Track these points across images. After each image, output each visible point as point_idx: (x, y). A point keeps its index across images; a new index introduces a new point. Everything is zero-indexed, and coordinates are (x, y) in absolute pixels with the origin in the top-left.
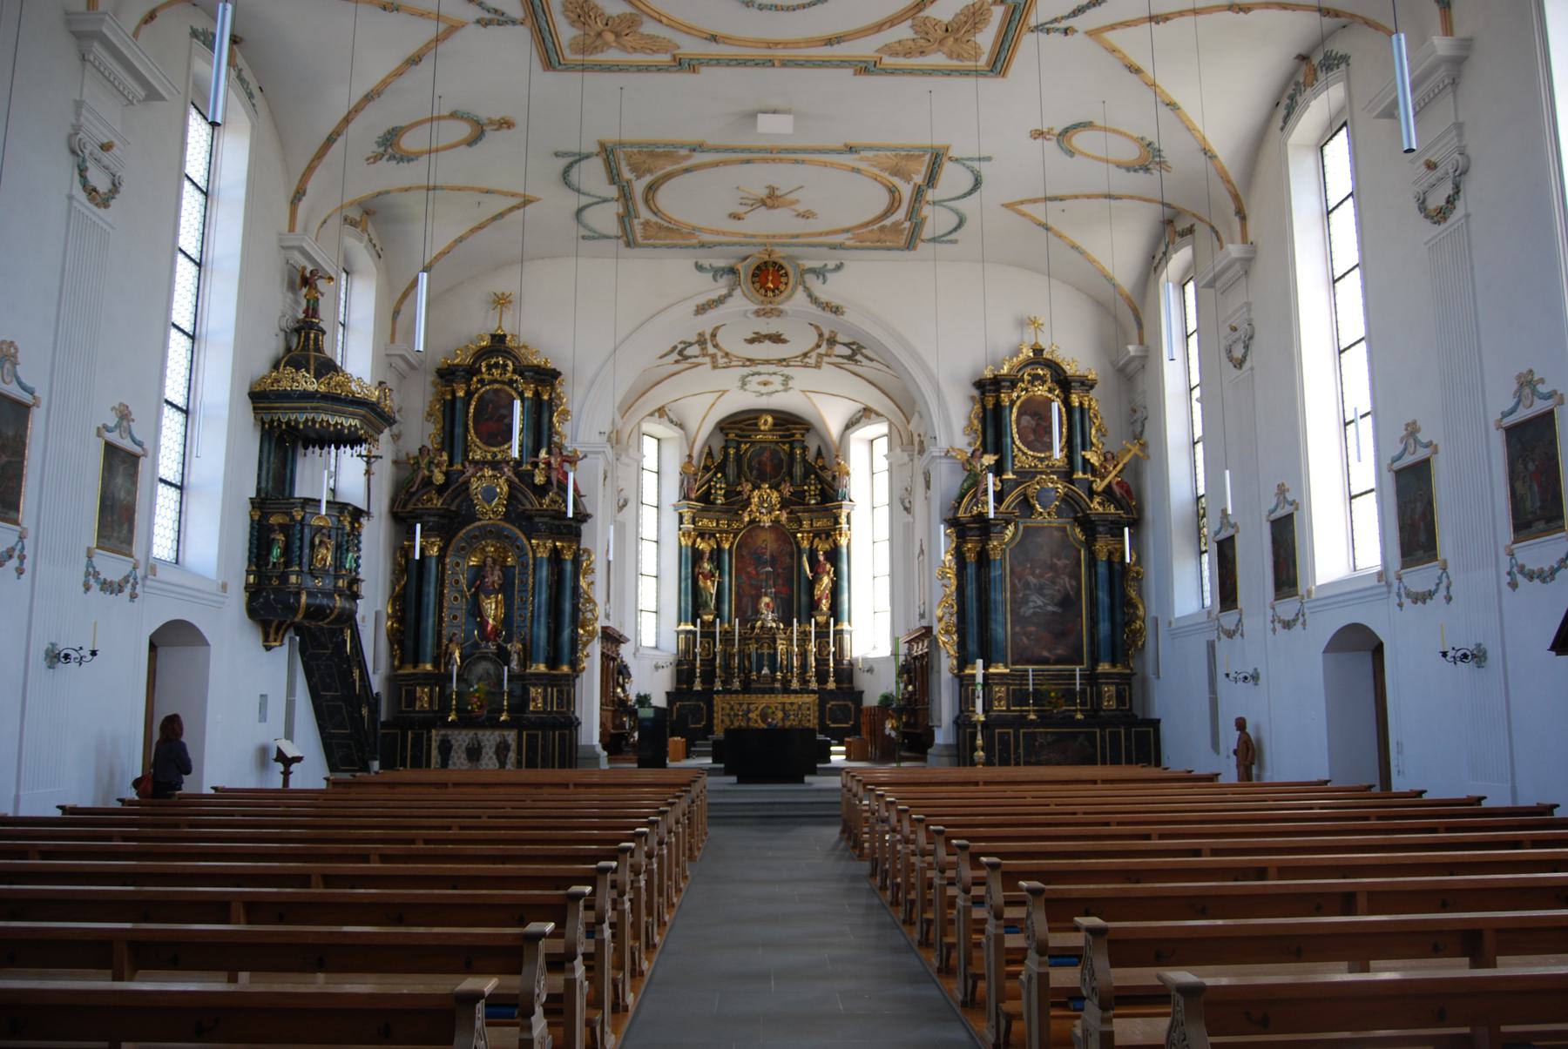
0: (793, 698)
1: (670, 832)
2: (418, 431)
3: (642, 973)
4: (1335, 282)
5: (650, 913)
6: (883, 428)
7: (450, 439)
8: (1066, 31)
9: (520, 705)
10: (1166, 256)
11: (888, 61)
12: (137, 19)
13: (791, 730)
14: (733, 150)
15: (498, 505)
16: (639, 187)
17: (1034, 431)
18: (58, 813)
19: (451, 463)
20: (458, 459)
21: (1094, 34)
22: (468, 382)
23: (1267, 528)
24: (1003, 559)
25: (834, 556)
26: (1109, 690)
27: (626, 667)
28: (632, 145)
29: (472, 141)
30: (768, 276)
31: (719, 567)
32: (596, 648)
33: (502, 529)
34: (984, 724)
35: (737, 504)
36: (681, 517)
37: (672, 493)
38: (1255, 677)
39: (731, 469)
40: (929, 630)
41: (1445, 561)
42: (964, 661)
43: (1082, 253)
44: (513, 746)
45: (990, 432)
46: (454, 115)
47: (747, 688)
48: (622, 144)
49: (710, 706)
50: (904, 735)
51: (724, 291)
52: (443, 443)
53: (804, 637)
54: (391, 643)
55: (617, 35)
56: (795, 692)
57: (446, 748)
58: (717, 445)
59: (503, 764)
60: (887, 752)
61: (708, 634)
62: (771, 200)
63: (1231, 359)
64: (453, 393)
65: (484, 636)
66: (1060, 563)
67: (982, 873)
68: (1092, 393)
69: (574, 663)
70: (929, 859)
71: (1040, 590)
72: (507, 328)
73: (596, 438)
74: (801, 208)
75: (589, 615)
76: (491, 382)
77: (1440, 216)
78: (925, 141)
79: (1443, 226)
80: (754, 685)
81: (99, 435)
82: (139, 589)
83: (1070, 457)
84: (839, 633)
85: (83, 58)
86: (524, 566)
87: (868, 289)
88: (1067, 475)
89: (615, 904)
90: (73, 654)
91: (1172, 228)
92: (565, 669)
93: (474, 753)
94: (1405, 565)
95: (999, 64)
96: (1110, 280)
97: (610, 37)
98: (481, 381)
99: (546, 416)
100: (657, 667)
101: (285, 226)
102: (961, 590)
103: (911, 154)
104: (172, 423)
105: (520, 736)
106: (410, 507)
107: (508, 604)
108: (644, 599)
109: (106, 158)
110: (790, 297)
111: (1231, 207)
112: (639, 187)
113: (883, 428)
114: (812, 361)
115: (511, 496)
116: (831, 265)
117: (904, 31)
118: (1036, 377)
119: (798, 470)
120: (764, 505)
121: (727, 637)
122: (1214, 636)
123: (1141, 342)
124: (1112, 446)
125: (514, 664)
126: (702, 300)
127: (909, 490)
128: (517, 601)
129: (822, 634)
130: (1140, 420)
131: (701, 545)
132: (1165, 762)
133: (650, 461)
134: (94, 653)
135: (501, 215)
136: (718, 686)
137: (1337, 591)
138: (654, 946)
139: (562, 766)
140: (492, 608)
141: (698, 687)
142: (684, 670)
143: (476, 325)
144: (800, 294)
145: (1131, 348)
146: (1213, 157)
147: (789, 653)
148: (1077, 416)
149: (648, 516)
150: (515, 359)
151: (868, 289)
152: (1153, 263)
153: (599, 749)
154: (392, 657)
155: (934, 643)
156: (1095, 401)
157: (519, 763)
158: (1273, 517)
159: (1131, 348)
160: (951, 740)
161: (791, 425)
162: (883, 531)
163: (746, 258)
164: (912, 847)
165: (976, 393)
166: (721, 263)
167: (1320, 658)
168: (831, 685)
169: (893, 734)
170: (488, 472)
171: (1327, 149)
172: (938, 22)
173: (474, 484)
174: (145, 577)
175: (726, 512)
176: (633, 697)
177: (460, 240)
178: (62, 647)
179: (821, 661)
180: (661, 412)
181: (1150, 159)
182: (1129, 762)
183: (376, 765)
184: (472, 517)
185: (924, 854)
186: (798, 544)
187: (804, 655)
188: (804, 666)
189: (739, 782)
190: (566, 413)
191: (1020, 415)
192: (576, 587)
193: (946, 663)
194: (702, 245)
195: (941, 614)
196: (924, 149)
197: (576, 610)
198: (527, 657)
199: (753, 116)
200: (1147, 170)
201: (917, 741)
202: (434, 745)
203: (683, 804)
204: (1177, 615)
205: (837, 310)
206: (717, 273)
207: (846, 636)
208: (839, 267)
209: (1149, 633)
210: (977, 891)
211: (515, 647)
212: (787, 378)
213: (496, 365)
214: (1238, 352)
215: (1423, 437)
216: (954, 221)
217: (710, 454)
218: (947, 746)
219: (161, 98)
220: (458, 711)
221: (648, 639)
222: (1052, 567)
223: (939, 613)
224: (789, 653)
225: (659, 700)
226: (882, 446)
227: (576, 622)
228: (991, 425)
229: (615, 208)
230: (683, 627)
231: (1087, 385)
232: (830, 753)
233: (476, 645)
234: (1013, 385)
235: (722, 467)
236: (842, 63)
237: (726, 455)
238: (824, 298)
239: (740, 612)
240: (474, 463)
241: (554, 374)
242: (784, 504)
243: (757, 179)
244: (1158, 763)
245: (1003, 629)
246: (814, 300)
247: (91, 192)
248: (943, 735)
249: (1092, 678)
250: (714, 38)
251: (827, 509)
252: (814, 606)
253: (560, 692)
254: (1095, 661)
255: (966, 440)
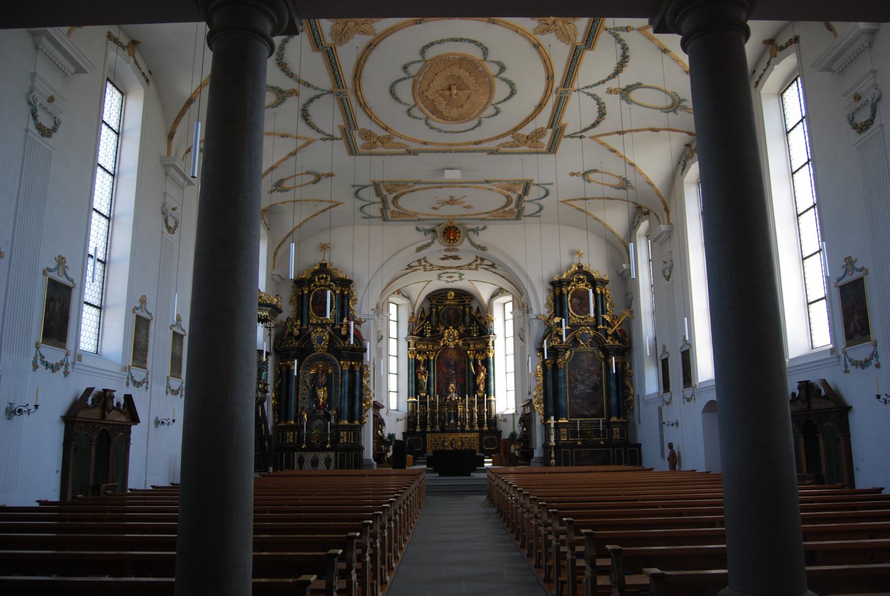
0: (466, 435)
1: (395, 514)
2: (288, 311)
3: (386, 583)
4: (793, 173)
5: (383, 563)
6: (510, 298)
7: (301, 313)
8: (581, 137)
9: (336, 440)
10: (638, 223)
11: (502, 149)
12: (185, 150)
13: (466, 450)
14: (434, 183)
15: (324, 345)
16: (390, 198)
17: (579, 305)
18: (37, 505)
19: (302, 325)
20: (305, 323)
21: (592, 138)
22: (309, 286)
23: (680, 355)
24: (565, 367)
25: (486, 362)
26: (616, 430)
27: (383, 420)
28: (388, 182)
29: (314, 183)
30: (451, 233)
31: (428, 369)
32: (371, 413)
33: (326, 356)
34: (555, 447)
35: (436, 336)
36: (409, 343)
37: (404, 332)
38: (677, 424)
39: (434, 319)
40: (531, 400)
41: (876, 341)
42: (546, 417)
43: (600, 221)
44: (333, 460)
45: (558, 307)
46: (307, 173)
47: (443, 430)
48: (383, 182)
49: (425, 439)
50: (522, 453)
51: (430, 241)
52: (297, 315)
53: (472, 403)
54: (274, 412)
55: (382, 143)
56: (467, 432)
57: (301, 461)
58: (427, 307)
59: (328, 468)
60: (512, 461)
61: (423, 402)
62: (452, 201)
63: (665, 276)
64: (302, 292)
65: (318, 407)
66: (592, 369)
67: (564, 528)
68: (607, 287)
69: (361, 420)
70: (549, 528)
71: (583, 382)
72: (327, 260)
73: (371, 312)
74: (465, 205)
75: (367, 397)
76: (320, 286)
77: (861, 128)
78: (520, 178)
79: (863, 135)
80: (447, 429)
81: (133, 312)
82: (70, 368)
83: (596, 316)
84: (489, 402)
85: (37, 47)
86: (337, 374)
87: (499, 238)
88: (595, 327)
89: (373, 545)
90: (24, 409)
91: (639, 212)
92: (357, 422)
93: (315, 463)
94: (685, 387)
95: (552, 148)
96: (613, 232)
97: (379, 144)
98: (315, 286)
99: (346, 302)
100: (398, 420)
101: (165, 154)
102: (545, 382)
103: (515, 183)
104: (93, 270)
105: (336, 455)
106: (283, 347)
107: (329, 392)
108: (392, 390)
109: (50, 107)
110: (461, 243)
111: (662, 207)
112: (390, 198)
113: (510, 298)
114: (473, 267)
115: (330, 341)
116: (481, 227)
117: (509, 139)
118: (579, 279)
119: (467, 319)
120: (451, 337)
121: (433, 403)
122: (661, 404)
123: (669, 223)
124: (616, 313)
125: (333, 421)
126: (420, 245)
127: (522, 330)
128: (334, 390)
129: (481, 402)
130: (630, 299)
131: (419, 358)
132: (646, 464)
133: (393, 316)
134: (174, 421)
135: (326, 210)
136: (429, 429)
137: (815, 359)
138: (393, 569)
139: (356, 468)
140: (322, 394)
141: (418, 430)
142: (411, 420)
143: (314, 259)
144: (466, 242)
145: (624, 265)
146: (652, 185)
147: (464, 412)
148: (599, 298)
149: (393, 344)
150: (331, 275)
151: (499, 238)
152: (633, 226)
153: (373, 461)
154: (274, 417)
155: (532, 408)
156: (608, 291)
157: (336, 468)
158: (842, 283)
159: (624, 265)
160: (541, 455)
161: (464, 296)
162: (510, 349)
163: (440, 225)
164: (539, 521)
165: (551, 287)
166: (428, 227)
167: (700, 415)
168: (486, 428)
169: (517, 453)
170: (320, 330)
171: (785, 95)
172: (523, 135)
173: (313, 336)
174: (73, 363)
175: (432, 341)
176: (386, 435)
177: (306, 220)
178: (16, 406)
179: (480, 416)
180: (399, 292)
181: (625, 184)
182: (614, 464)
183: (271, 469)
184: (312, 350)
185: (546, 525)
186: (468, 356)
187: (471, 412)
188: (472, 418)
189: (440, 476)
190: (356, 300)
191: (572, 297)
192: (361, 383)
193: (538, 418)
194: (419, 220)
195: (536, 394)
196: (522, 181)
197: (361, 394)
198: (339, 417)
199: (442, 170)
200: (674, 111)
201: (527, 456)
202: (296, 459)
203: (416, 483)
204: (647, 393)
205: (484, 249)
206: (426, 232)
207: (493, 403)
208: (484, 228)
209: (635, 402)
210: (562, 537)
211: (333, 412)
212: (461, 275)
213: (322, 278)
214: (667, 274)
215: (858, 265)
216: (538, 208)
217: (423, 312)
218: (539, 458)
219: (84, 71)
220: (307, 443)
221: (393, 405)
222: (589, 371)
223: (535, 393)
224: (464, 412)
225: (399, 437)
226: (509, 307)
227: (362, 400)
228: (558, 304)
229: (380, 206)
230: (410, 399)
231: (604, 283)
232: (484, 462)
233: (314, 412)
234: (568, 283)
235: (429, 318)
236: (482, 151)
237: (431, 312)
238: (477, 243)
239: (439, 392)
240: (312, 324)
241: (350, 282)
242: (461, 336)
243: (445, 194)
244: (641, 464)
245: (565, 401)
246: (473, 244)
247: (39, 127)
248: (538, 453)
249: (608, 424)
250: (425, 143)
251: (482, 339)
252: (476, 388)
253: (355, 434)
254: (610, 416)
255: (546, 310)
